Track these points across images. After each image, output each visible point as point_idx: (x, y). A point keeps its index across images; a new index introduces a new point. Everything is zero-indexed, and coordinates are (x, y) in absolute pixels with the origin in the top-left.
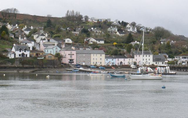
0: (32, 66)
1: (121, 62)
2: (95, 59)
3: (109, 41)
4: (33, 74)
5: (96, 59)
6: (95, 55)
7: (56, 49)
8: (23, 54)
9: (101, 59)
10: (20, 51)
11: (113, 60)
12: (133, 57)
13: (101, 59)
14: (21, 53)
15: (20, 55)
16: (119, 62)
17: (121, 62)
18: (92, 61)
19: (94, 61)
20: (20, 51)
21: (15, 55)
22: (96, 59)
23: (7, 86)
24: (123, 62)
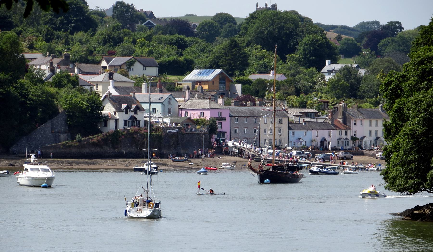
10: (126, 113)
14: (127, 117)
16: (319, 140)
20: (126, 113)
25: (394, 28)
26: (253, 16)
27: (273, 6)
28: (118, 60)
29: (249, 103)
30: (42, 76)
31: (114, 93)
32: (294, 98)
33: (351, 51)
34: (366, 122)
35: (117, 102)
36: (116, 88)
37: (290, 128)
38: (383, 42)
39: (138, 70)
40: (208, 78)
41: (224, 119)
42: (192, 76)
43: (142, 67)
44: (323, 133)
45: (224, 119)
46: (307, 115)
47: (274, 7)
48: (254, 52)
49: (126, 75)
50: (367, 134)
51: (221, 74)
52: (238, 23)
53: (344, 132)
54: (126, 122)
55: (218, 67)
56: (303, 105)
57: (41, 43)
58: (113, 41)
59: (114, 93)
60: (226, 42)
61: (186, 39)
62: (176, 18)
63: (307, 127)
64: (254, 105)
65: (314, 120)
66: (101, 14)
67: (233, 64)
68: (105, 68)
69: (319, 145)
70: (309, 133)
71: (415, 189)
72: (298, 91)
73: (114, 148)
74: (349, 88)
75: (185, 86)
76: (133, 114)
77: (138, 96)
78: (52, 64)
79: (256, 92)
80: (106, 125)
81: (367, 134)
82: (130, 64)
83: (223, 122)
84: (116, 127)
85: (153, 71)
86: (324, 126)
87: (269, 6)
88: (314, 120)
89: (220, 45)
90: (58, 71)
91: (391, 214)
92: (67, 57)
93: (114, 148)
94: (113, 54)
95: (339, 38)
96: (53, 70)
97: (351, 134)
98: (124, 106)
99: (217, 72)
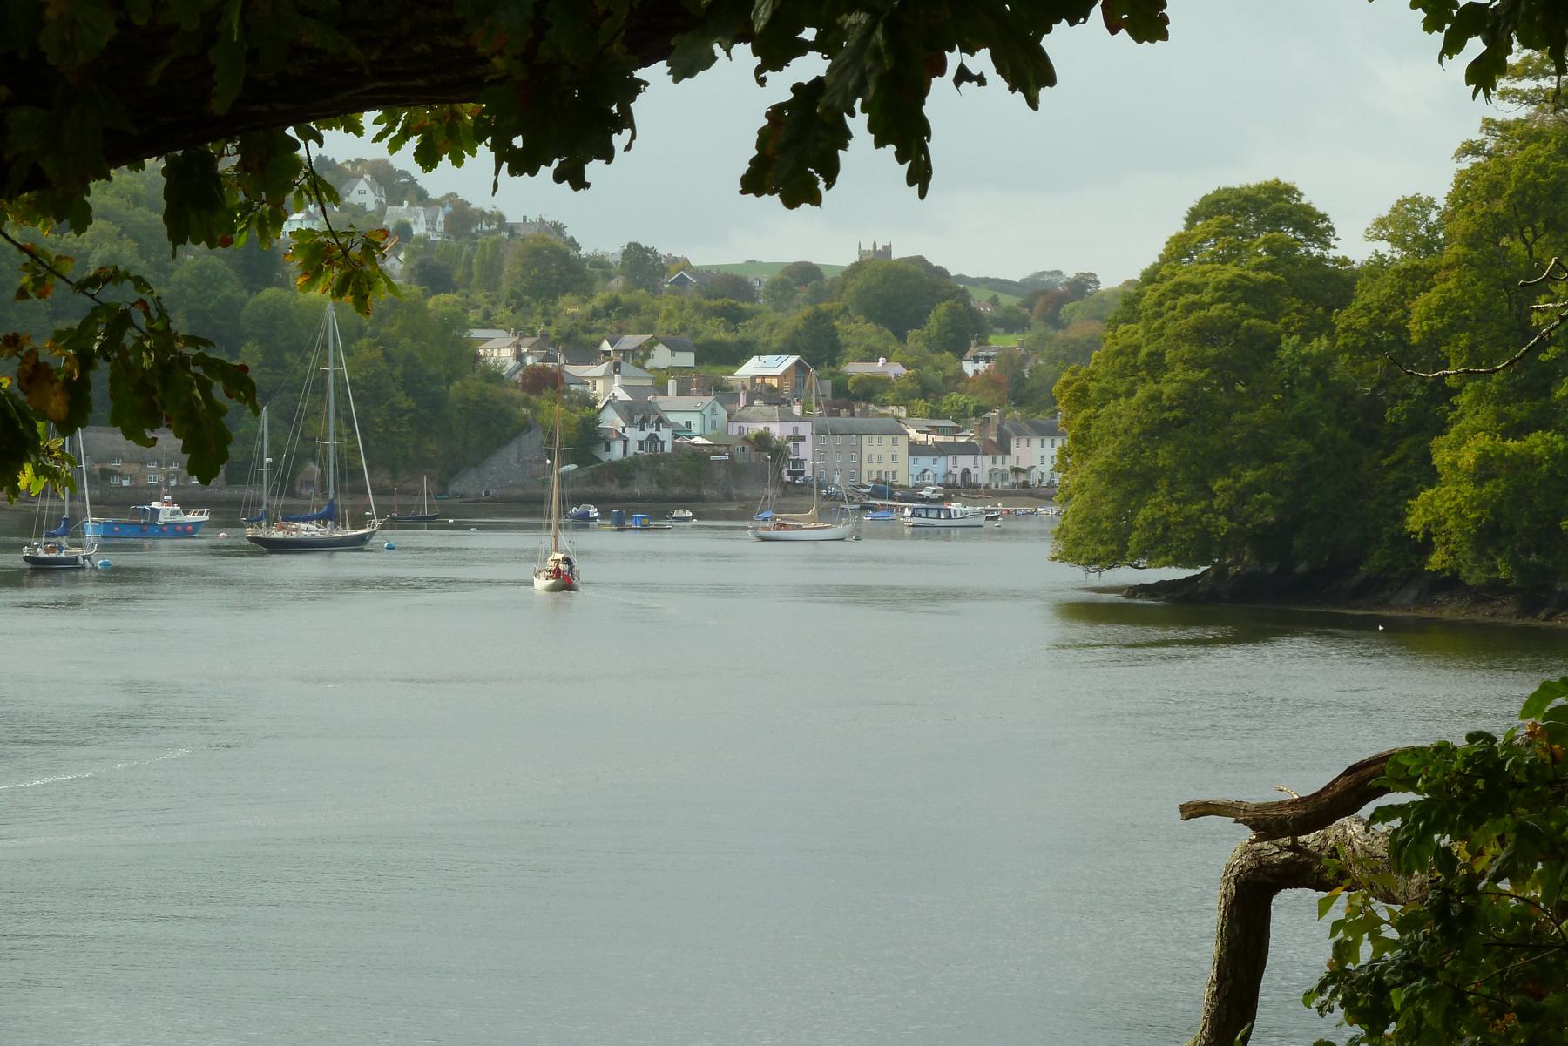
0: (691, 492)
1: (966, 472)
2: (875, 459)
3: (599, 323)
4: (354, 528)
5: (879, 457)
6: (875, 438)
7: (713, 411)
8: (653, 439)
9: (894, 457)
10: (642, 429)
11: (935, 462)
12: (1003, 448)
13: (894, 457)
14: (643, 435)
15: (641, 443)
16: (958, 471)
17: (966, 472)
18: (866, 467)
19: (871, 467)
20: (642, 429)
21: (626, 441)
22: (879, 457)
23: (956, 595)
24: (974, 471)
25: (1082, 286)
26: (857, 268)
27: (885, 247)
28: (631, 341)
29: (843, 412)
30: (502, 367)
31: (623, 396)
32: (920, 404)
33: (1011, 323)
34: (1036, 442)
35: (629, 412)
36: (625, 387)
37: (911, 453)
38: (1068, 307)
39: (662, 357)
40: (779, 371)
41: (803, 439)
42: (753, 367)
43: (668, 352)
44: (966, 461)
45: (803, 439)
46: (936, 430)
47: (887, 251)
48: (856, 330)
49: (641, 366)
50: (1036, 462)
51: (797, 363)
52: (828, 275)
53: (999, 458)
54: (641, 443)
55: (791, 353)
56: (935, 414)
57: (502, 313)
58: (619, 313)
59: (623, 396)
60: (807, 310)
61: (741, 305)
62: (718, 267)
63: (940, 450)
64: (852, 415)
65: (951, 439)
66: (599, 263)
67: (817, 346)
68: (607, 353)
69: (958, 480)
70: (942, 460)
71: (1116, 558)
72: (926, 393)
73: (623, 486)
74: (1022, 395)
75: (358, 258)
76: (653, 430)
77: (663, 402)
78: (518, 347)
79: (852, 396)
80: (608, 449)
81: (1036, 462)
82: (651, 345)
83: (801, 444)
84: (625, 452)
85: (686, 359)
86: (969, 449)
87: (879, 248)
88: (951, 439)
89: (795, 318)
90: (529, 361)
91: (956, 595)
92: (545, 336)
93: (623, 486)
94: (621, 331)
95: (994, 301)
96: (519, 357)
97: (1011, 462)
98: (637, 418)
99: (793, 359)
